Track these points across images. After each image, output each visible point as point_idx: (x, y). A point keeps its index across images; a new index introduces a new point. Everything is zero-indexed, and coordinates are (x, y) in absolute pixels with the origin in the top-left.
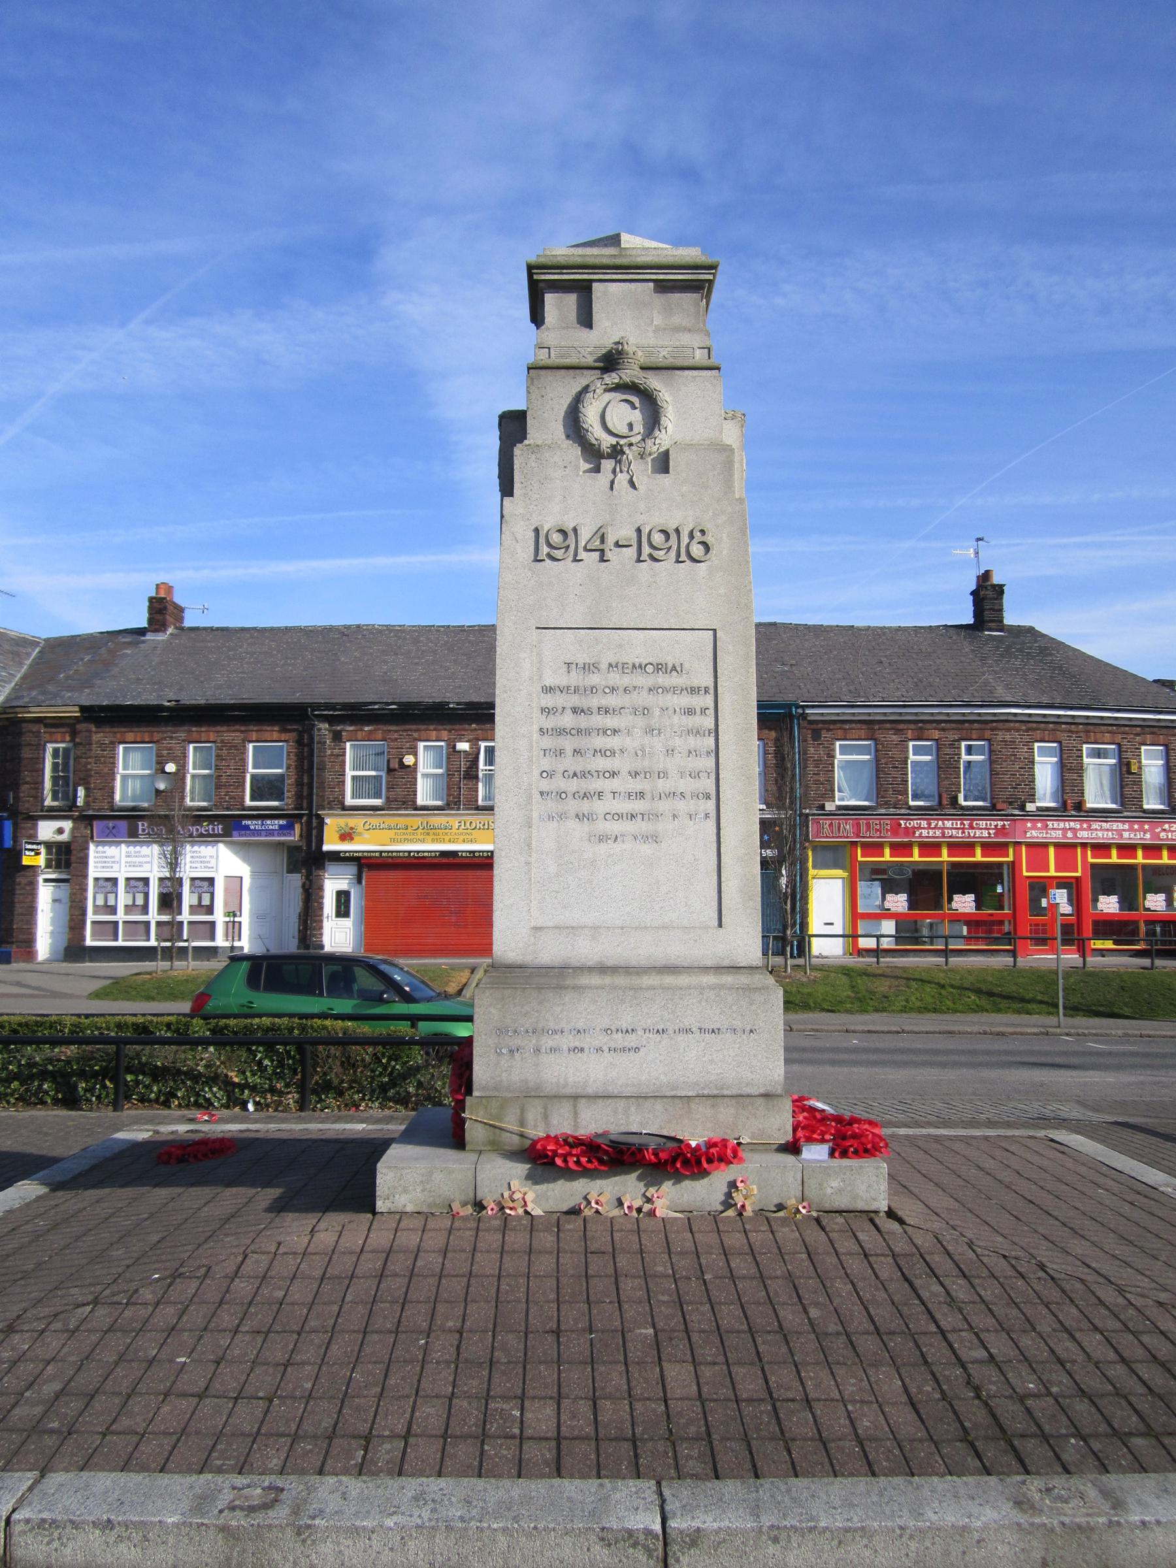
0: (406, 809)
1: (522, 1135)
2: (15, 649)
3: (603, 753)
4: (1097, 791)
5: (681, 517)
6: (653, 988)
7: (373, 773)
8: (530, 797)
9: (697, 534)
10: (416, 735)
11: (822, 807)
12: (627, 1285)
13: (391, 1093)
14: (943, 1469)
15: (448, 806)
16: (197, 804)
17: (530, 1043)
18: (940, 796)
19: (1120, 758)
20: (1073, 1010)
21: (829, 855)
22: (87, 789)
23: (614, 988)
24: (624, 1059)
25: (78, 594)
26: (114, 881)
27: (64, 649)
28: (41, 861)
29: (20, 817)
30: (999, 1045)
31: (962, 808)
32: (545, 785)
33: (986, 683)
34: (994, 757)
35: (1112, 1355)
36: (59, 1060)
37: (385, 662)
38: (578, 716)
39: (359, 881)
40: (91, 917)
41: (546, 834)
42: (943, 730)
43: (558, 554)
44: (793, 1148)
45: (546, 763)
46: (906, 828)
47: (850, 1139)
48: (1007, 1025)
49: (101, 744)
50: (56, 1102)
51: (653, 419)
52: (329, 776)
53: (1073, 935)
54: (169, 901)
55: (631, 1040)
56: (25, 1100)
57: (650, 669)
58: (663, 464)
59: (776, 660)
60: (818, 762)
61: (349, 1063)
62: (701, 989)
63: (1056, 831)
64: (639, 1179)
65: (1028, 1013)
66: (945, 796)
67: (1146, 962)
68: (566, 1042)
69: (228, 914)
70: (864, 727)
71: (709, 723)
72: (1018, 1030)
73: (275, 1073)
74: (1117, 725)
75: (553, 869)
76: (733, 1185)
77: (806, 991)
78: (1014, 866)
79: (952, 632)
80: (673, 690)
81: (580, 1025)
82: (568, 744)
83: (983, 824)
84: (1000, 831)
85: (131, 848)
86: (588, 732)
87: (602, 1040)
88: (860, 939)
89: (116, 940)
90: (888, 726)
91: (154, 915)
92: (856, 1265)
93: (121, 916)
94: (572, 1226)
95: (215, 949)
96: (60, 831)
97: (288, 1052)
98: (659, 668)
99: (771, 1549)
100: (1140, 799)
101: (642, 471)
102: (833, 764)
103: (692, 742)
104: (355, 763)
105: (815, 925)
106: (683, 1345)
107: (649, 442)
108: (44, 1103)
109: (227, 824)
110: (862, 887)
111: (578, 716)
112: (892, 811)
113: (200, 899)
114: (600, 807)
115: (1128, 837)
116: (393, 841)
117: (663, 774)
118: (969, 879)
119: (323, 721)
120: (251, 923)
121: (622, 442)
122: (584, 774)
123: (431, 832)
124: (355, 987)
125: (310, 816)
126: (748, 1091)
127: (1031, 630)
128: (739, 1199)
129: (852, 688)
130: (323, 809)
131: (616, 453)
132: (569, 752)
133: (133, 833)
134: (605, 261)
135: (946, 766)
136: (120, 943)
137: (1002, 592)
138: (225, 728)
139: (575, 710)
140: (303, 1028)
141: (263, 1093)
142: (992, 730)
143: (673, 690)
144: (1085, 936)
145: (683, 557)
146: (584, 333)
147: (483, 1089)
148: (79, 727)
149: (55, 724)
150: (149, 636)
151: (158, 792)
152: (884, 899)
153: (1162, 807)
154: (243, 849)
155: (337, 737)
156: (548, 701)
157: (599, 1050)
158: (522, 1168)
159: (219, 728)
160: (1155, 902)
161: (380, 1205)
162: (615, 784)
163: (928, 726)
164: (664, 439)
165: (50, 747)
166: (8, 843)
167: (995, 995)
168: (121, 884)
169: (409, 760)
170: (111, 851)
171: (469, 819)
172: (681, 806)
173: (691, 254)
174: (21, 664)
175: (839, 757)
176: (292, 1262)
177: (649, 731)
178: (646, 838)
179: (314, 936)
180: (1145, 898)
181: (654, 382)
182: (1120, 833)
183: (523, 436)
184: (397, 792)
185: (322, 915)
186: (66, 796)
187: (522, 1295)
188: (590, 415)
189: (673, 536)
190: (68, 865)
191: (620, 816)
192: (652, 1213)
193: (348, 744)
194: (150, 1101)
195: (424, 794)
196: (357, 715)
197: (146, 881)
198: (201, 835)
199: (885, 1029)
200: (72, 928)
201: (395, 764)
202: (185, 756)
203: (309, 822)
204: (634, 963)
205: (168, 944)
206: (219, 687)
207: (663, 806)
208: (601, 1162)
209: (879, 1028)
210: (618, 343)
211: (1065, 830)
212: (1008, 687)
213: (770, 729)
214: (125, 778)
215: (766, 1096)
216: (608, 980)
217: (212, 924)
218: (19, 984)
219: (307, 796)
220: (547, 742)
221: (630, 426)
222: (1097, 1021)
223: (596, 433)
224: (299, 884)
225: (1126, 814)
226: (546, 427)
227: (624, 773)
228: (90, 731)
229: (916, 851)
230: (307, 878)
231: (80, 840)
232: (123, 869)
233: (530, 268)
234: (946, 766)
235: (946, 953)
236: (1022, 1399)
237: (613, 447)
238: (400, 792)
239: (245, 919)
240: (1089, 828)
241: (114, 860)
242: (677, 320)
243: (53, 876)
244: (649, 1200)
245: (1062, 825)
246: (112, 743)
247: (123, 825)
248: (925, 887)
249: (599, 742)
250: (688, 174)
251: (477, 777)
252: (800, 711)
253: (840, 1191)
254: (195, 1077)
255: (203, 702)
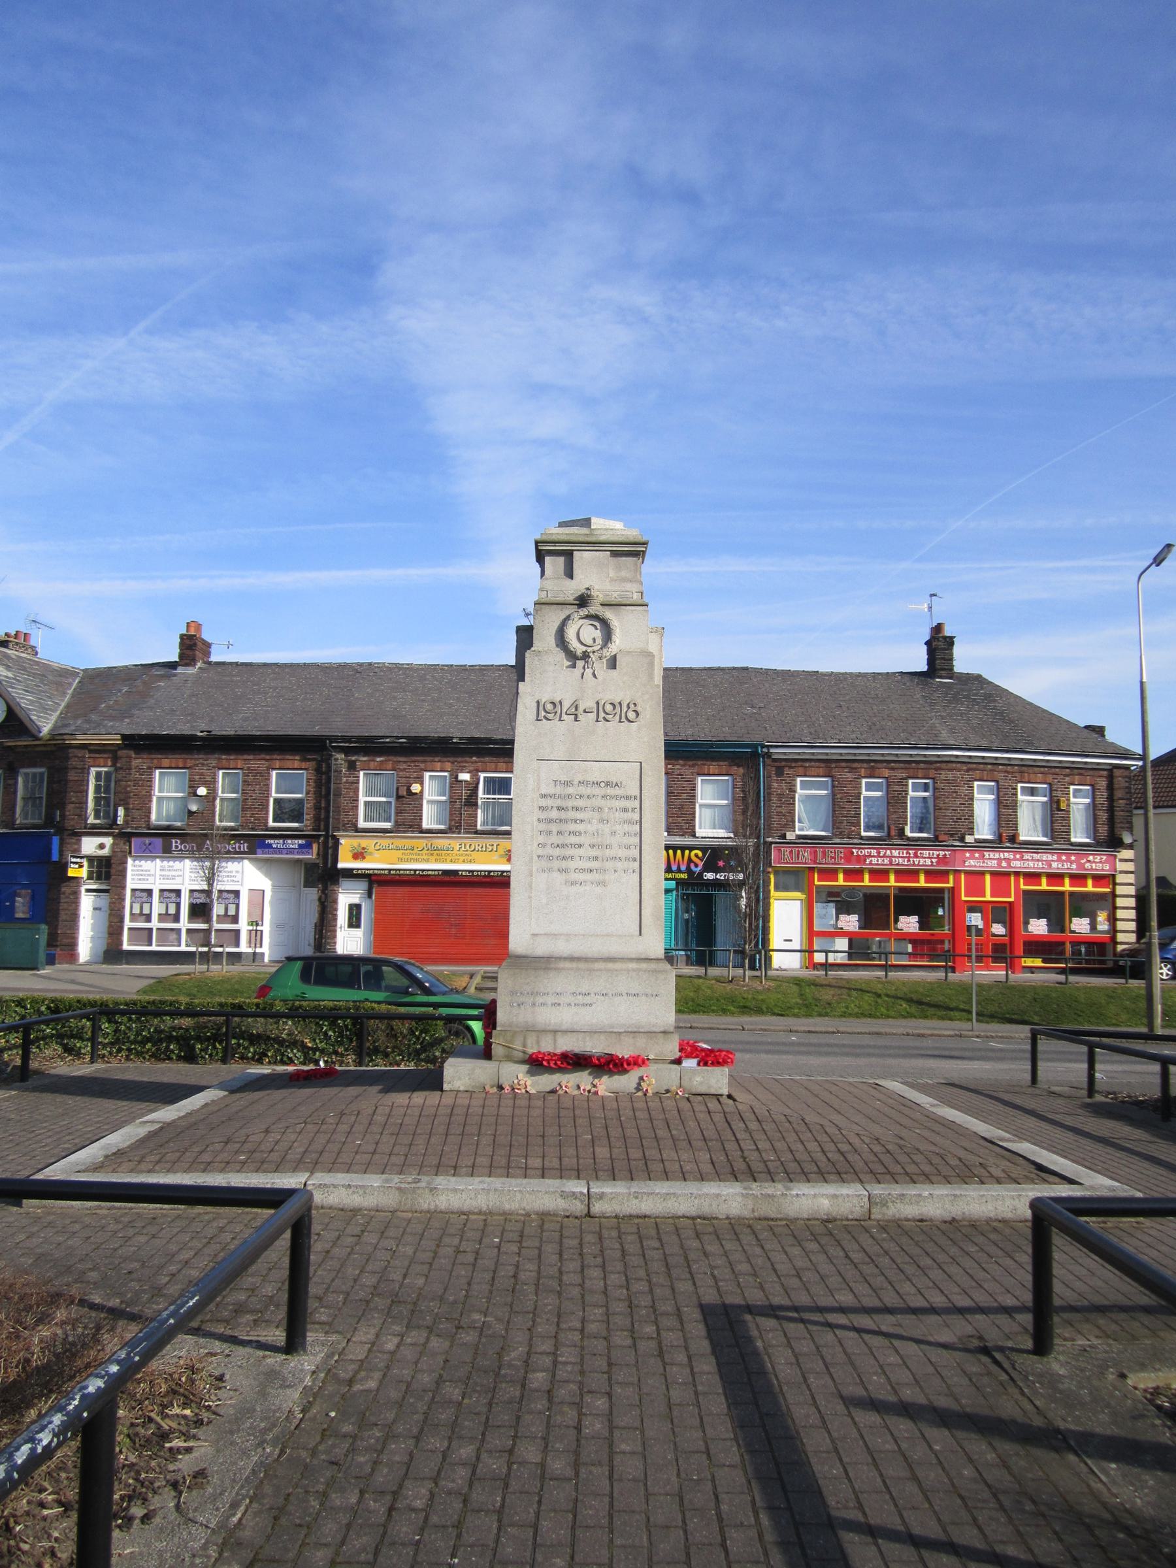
0: (413, 832)
1: (524, 1052)
2: (58, 679)
3: (575, 833)
4: (1029, 827)
5: (622, 695)
6: (600, 970)
7: (384, 799)
8: (532, 858)
9: (632, 706)
10: (422, 766)
11: (784, 836)
12: (579, 1121)
13: (423, 1056)
14: (707, 1168)
15: (450, 830)
16: (225, 824)
17: (530, 1000)
18: (889, 828)
19: (1051, 797)
20: (983, 1016)
21: (791, 880)
22: (126, 809)
23: (578, 969)
24: (582, 1010)
25: (95, 619)
26: (149, 892)
27: (100, 681)
28: (83, 873)
29: (66, 833)
30: (917, 1043)
31: (909, 839)
32: (540, 852)
33: (932, 727)
34: (937, 794)
35: (819, 1149)
36: (181, 1028)
37: (395, 698)
38: (560, 811)
39: (370, 896)
40: (128, 923)
41: (541, 880)
42: (893, 769)
43: (550, 716)
44: (678, 1062)
45: (541, 839)
46: (858, 856)
47: (710, 1058)
48: (929, 1028)
49: (139, 769)
50: (179, 1058)
51: (608, 636)
52: (343, 802)
53: (1002, 953)
54: (200, 911)
55: (588, 1000)
56: (156, 1057)
57: (603, 784)
58: (613, 663)
59: (746, 703)
60: (780, 796)
61: (392, 1034)
62: (628, 971)
63: (992, 861)
64: (590, 1074)
65: (951, 1019)
66: (893, 827)
67: (1062, 978)
68: (550, 999)
69: (251, 923)
70: (823, 765)
71: (636, 817)
72: (936, 1032)
73: (336, 1041)
74: (1049, 767)
75: (544, 901)
76: (641, 1078)
77: (760, 997)
78: (953, 891)
79: (906, 678)
80: (616, 797)
81: (558, 990)
82: (554, 828)
83: (926, 853)
84: (942, 860)
85: (165, 863)
86: (566, 821)
87: (571, 999)
88: (816, 954)
89: (150, 945)
90: (844, 764)
91: (184, 923)
92: (702, 1116)
93: (155, 924)
94: (551, 1097)
95: (239, 955)
96: (102, 846)
97: (346, 1026)
98: (608, 784)
99: (635, 1201)
100: (1068, 833)
101: (600, 667)
102: (794, 798)
103: (626, 827)
104: (367, 791)
105: (776, 941)
106: (606, 1142)
107: (605, 650)
108: (170, 1059)
109: (253, 842)
110: (818, 908)
111: (560, 811)
112: (846, 840)
113: (226, 909)
114: (572, 865)
115: (1056, 867)
116: (400, 860)
117: (609, 846)
118: (911, 902)
119: (339, 752)
120: (271, 932)
121: (589, 650)
122: (564, 846)
123: (434, 852)
124: (383, 984)
125: (327, 836)
126: (654, 1029)
127: (979, 678)
128: (644, 1086)
129: (812, 730)
130: (339, 830)
131: (585, 656)
132: (555, 832)
133: (167, 850)
134: (581, 539)
135: (895, 800)
136: (154, 948)
137: (952, 644)
138: (251, 757)
139: (558, 808)
140: (357, 1009)
141: (330, 1055)
142: (936, 769)
143: (616, 797)
144: (1017, 954)
145: (623, 719)
146: (568, 582)
147: (502, 1026)
148: (120, 753)
149: (99, 750)
150: (180, 670)
151: (191, 813)
152: (837, 919)
153: (1088, 840)
154: (266, 865)
155: (352, 767)
156: (544, 802)
157: (569, 1005)
158: (525, 1067)
159: (246, 757)
160: (1080, 925)
161: (446, 1087)
162: (581, 852)
163: (879, 765)
164: (613, 648)
165: (93, 770)
166: (55, 857)
167: (924, 1004)
168: (156, 895)
169: (416, 788)
170: (147, 865)
171: (469, 841)
172: (619, 865)
173: (633, 533)
174: (65, 693)
175: (800, 792)
176: (402, 1110)
177: (602, 821)
178: (598, 883)
179: (329, 944)
180: (1071, 922)
181: (608, 614)
182: (1049, 863)
183: (531, 645)
184: (406, 818)
185: (336, 926)
186: (107, 816)
187: (525, 1123)
188: (571, 633)
189: (618, 707)
190: (108, 877)
191: (583, 870)
192: (596, 1093)
193: (362, 773)
194: (247, 1058)
195: (429, 819)
196: (370, 747)
197: (178, 892)
198: (228, 852)
199: (823, 1029)
200: (110, 934)
201: (403, 792)
202: (215, 781)
203: (326, 843)
204: (590, 955)
205: (205, 949)
206: (245, 719)
207: (609, 865)
208: (569, 1064)
209: (817, 1029)
210: (588, 589)
211: (999, 860)
212: (952, 731)
213: (739, 766)
214: (160, 799)
215: (664, 1032)
216: (574, 965)
217: (237, 932)
218: (73, 982)
219: (325, 819)
220: (542, 827)
221: (594, 640)
222: (1008, 1027)
223: (574, 645)
224: (316, 897)
225: (1055, 846)
226: (544, 639)
227: (586, 845)
228: (130, 757)
229: (866, 876)
230: (323, 892)
231: (120, 855)
232: (158, 881)
233: (537, 543)
234: (895, 800)
235: (885, 968)
236: (765, 1162)
237: (584, 652)
238: (407, 817)
239: (266, 928)
240: (1021, 859)
241: (146, 873)
242: (624, 574)
243: (94, 887)
244: (595, 1086)
245: (997, 856)
246: (150, 768)
247: (158, 842)
248: (875, 909)
249: (573, 827)
250: (688, 196)
251: (476, 805)
252: (765, 750)
253: (701, 1083)
254: (281, 1042)
255: (232, 733)
